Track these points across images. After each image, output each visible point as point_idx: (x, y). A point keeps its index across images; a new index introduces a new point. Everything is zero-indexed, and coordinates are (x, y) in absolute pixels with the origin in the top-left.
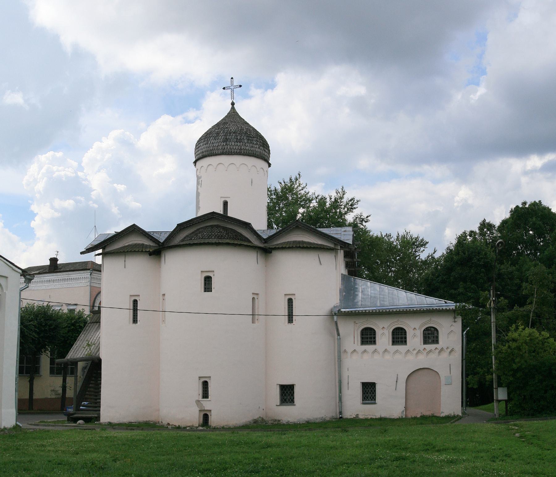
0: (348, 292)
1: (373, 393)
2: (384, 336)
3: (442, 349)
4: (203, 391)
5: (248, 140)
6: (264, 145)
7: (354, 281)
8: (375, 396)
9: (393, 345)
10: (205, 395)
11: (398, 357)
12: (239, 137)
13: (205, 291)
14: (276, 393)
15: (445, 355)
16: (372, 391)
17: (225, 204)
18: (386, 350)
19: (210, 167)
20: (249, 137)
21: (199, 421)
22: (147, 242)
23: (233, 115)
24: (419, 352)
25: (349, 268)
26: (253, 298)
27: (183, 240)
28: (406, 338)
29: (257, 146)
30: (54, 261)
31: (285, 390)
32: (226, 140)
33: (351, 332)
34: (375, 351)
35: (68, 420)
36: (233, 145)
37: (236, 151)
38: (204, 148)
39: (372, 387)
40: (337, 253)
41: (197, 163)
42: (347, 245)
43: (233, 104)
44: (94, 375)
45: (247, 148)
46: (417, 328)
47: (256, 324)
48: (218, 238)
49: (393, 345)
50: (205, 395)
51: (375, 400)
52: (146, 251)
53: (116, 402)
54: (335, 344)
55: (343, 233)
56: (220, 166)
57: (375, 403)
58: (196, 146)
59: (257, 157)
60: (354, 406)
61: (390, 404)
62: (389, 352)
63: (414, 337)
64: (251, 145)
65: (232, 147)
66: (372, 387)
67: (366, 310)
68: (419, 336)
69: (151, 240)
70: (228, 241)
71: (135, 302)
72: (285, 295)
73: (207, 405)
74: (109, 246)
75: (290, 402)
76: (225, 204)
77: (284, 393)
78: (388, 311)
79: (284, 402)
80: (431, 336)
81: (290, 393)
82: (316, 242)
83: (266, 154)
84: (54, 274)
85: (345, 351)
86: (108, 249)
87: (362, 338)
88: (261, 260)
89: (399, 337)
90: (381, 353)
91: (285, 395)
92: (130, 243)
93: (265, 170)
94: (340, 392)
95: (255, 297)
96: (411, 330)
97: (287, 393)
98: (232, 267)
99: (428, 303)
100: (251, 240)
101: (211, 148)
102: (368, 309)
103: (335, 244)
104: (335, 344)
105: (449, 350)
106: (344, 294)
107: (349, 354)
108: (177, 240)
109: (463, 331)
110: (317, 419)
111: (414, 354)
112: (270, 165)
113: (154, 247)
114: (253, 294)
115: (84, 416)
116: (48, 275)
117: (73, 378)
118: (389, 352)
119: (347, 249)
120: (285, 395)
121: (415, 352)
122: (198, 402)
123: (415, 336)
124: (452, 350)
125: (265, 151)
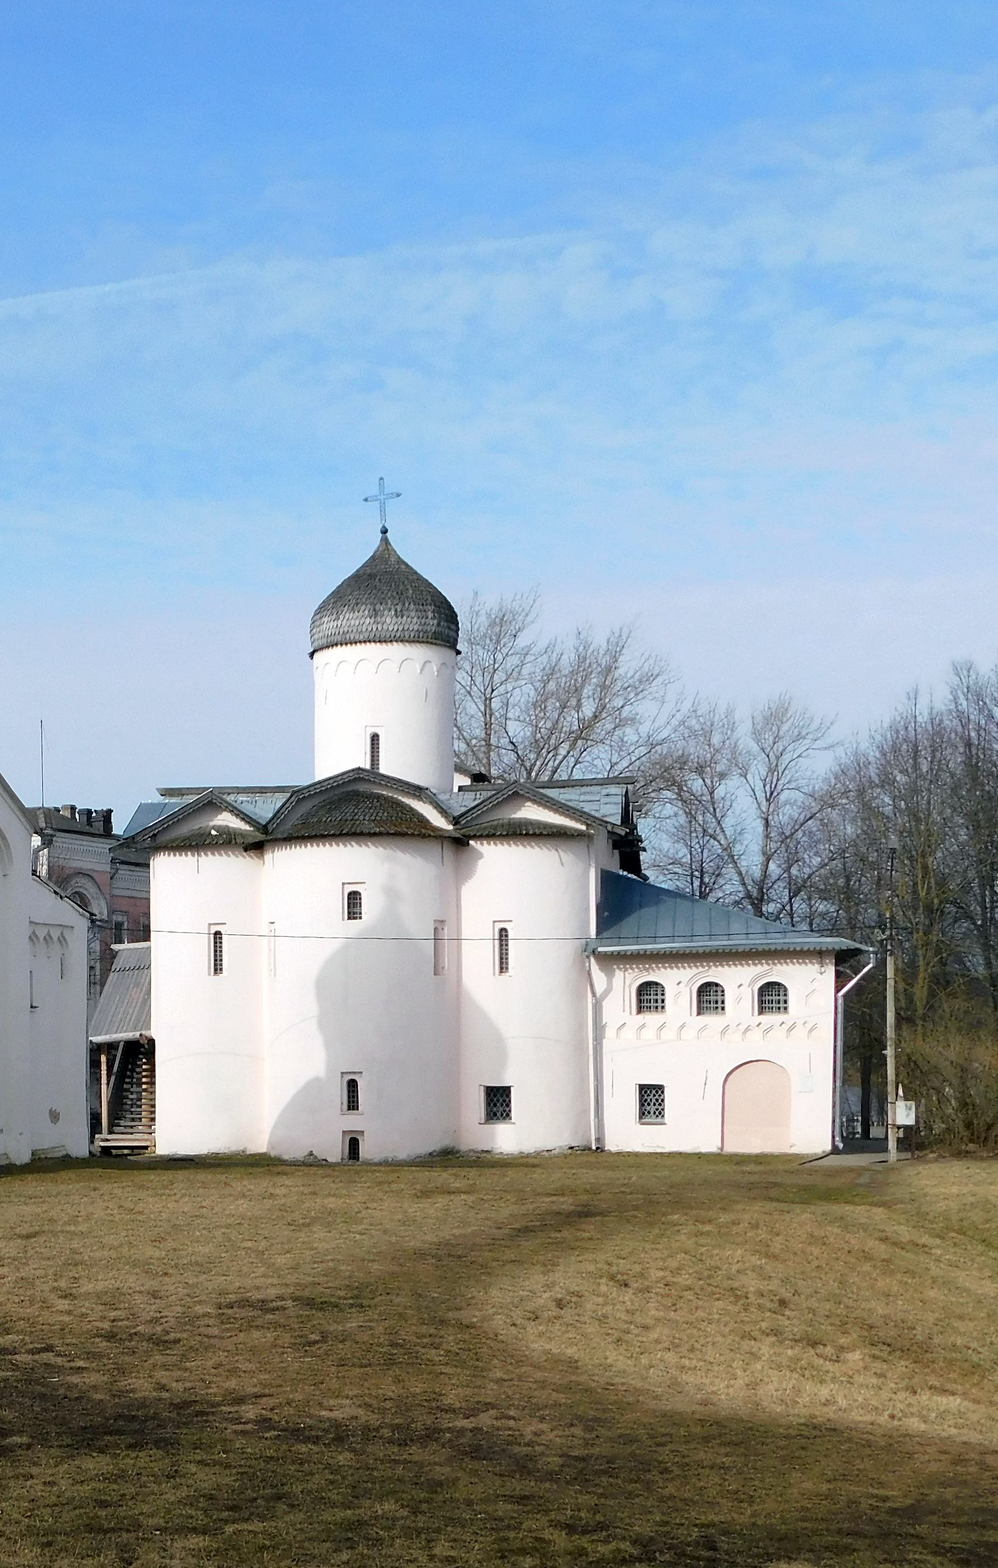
1: (660, 1105)
10: (353, 1103)
14: (476, 1104)
16: (657, 1100)
26: (435, 929)
41: (316, 656)
43: (384, 531)
44: (127, 1080)
50: (353, 1103)
55: (604, 800)
60: (625, 1133)
88: (448, 852)
89: (709, 997)
91: (495, 1105)
108: (185, 830)
109: (838, 990)
114: (435, 921)
120: (495, 1105)
125: (449, 628)
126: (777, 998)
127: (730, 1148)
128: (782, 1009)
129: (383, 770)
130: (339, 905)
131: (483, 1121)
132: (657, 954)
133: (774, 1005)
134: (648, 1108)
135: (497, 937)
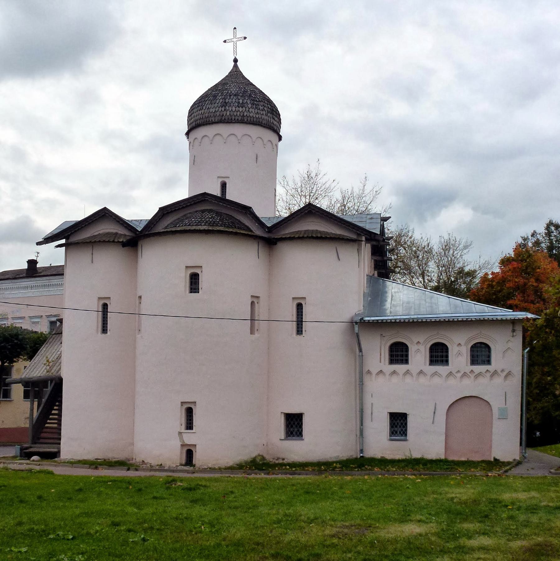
0: (376, 297)
1: (404, 427)
2: (419, 355)
3: (495, 372)
4: (187, 420)
5: (253, 104)
6: (274, 111)
7: (383, 283)
8: (406, 430)
9: (430, 364)
10: (189, 425)
11: (437, 380)
12: (241, 101)
13: (191, 292)
14: (279, 425)
15: (498, 380)
16: (402, 424)
17: (224, 186)
18: (421, 372)
19: (206, 138)
20: (253, 100)
21: (181, 458)
22: (121, 231)
23: (235, 73)
24: (465, 374)
25: (379, 269)
26: (252, 303)
27: (166, 228)
28: (447, 356)
29: (264, 112)
30: (32, 263)
31: (292, 420)
32: (225, 104)
33: (376, 350)
34: (407, 372)
35: (21, 456)
36: (233, 110)
37: (237, 118)
38: (198, 114)
39: (402, 418)
40: (360, 245)
42: (373, 235)
43: (236, 61)
45: (251, 115)
46: (463, 343)
47: (257, 335)
48: (209, 225)
49: (430, 364)
50: (189, 425)
51: (406, 435)
52: (118, 242)
53: (81, 434)
54: (356, 362)
55: (368, 221)
56: (218, 137)
57: (406, 440)
58: (189, 113)
59: (264, 127)
60: (379, 443)
61: (427, 441)
62: (425, 374)
63: (459, 355)
64: (256, 111)
65: (232, 113)
66: (402, 418)
67: (396, 319)
68: (465, 355)
69: (126, 227)
70: (222, 228)
71: (105, 306)
72: (293, 298)
73: (190, 438)
74: (70, 235)
75: (298, 436)
76: (224, 186)
77: (290, 423)
78: (424, 320)
79: (289, 436)
80: (480, 354)
81: (298, 424)
82: (333, 232)
83: (275, 123)
84: (33, 279)
85: (369, 372)
86: (73, 239)
87: (391, 356)
88: (263, 251)
89: (439, 355)
90: (401, 375)
91: (292, 426)
92: (101, 232)
93: (274, 144)
94: (362, 424)
95: (255, 301)
96: (455, 346)
97: (294, 424)
98: (230, 266)
99: (478, 310)
100: (252, 228)
101: (207, 115)
102: (398, 317)
103: (359, 235)
104: (356, 362)
105: (505, 373)
106: (369, 299)
107: (374, 375)
108: (160, 228)
110: (331, 458)
111: (459, 377)
112: (280, 138)
113: (132, 238)
114: (252, 296)
115: (41, 450)
116: (26, 280)
117: (29, 403)
118: (425, 374)
119: (374, 243)
120: (292, 426)
121: (459, 375)
122: (180, 433)
123: (459, 354)
124: (509, 374)
125: (273, 119)
126: (401, 353)
127: (451, 458)
128: (404, 361)
129: (228, 197)
130: (184, 283)
131: (283, 438)
132: (409, 322)
133: (399, 358)
134: (396, 429)
135: (100, 309)
